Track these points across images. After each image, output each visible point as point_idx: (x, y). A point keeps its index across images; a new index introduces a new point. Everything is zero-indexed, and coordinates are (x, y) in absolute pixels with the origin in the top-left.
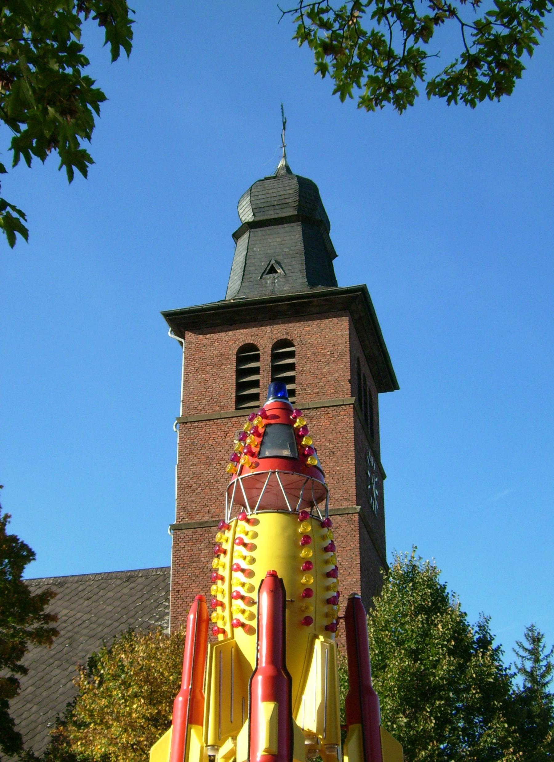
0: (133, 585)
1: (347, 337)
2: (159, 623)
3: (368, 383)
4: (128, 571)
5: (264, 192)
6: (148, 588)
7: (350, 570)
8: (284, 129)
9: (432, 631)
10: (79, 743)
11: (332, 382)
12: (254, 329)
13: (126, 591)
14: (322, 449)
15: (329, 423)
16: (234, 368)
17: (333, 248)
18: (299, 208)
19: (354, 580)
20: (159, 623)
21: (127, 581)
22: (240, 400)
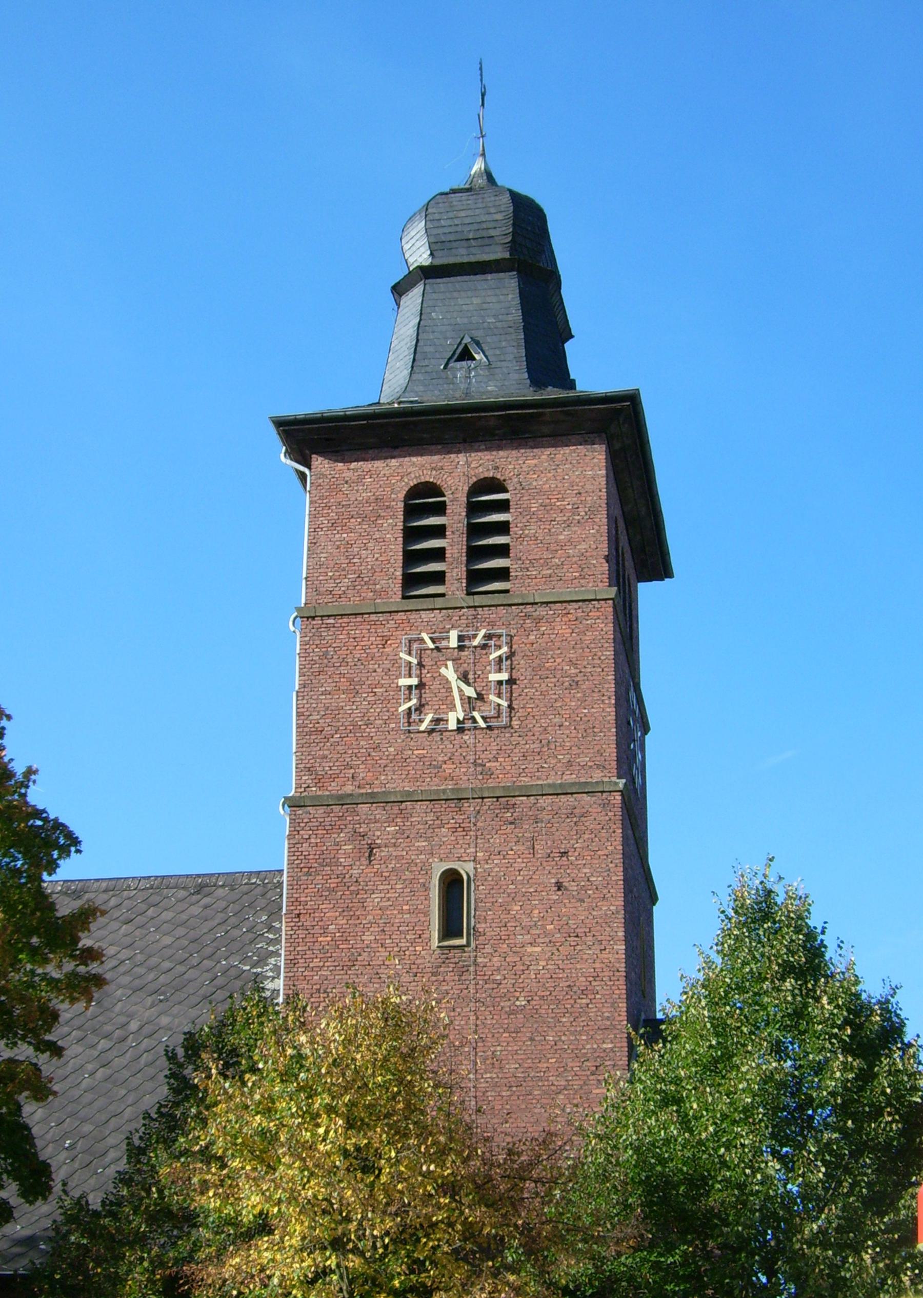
0: (207, 900)
1: (603, 481)
2: (259, 970)
3: (626, 563)
4: (199, 876)
5: (451, 215)
6: (237, 907)
7: (605, 891)
8: (483, 104)
9: (810, 1009)
10: (211, 1194)
11: (574, 559)
12: (436, 458)
13: (195, 910)
14: (558, 676)
15: (570, 631)
16: (400, 525)
17: (567, 321)
18: (514, 246)
19: (612, 908)
20: (259, 970)
21: (198, 892)
22: (411, 581)
